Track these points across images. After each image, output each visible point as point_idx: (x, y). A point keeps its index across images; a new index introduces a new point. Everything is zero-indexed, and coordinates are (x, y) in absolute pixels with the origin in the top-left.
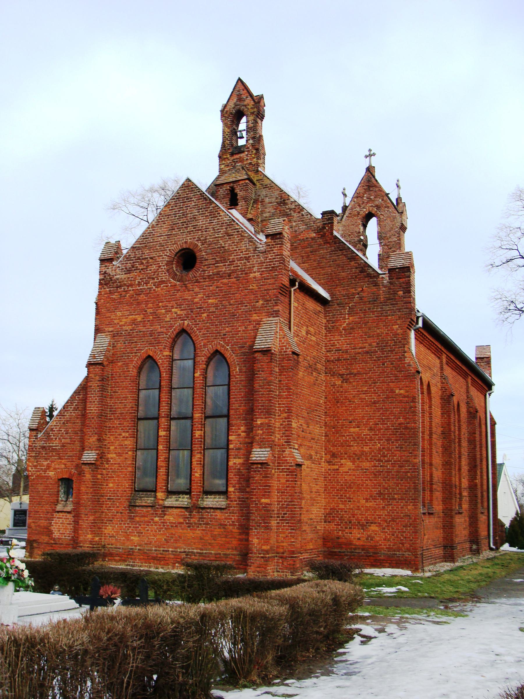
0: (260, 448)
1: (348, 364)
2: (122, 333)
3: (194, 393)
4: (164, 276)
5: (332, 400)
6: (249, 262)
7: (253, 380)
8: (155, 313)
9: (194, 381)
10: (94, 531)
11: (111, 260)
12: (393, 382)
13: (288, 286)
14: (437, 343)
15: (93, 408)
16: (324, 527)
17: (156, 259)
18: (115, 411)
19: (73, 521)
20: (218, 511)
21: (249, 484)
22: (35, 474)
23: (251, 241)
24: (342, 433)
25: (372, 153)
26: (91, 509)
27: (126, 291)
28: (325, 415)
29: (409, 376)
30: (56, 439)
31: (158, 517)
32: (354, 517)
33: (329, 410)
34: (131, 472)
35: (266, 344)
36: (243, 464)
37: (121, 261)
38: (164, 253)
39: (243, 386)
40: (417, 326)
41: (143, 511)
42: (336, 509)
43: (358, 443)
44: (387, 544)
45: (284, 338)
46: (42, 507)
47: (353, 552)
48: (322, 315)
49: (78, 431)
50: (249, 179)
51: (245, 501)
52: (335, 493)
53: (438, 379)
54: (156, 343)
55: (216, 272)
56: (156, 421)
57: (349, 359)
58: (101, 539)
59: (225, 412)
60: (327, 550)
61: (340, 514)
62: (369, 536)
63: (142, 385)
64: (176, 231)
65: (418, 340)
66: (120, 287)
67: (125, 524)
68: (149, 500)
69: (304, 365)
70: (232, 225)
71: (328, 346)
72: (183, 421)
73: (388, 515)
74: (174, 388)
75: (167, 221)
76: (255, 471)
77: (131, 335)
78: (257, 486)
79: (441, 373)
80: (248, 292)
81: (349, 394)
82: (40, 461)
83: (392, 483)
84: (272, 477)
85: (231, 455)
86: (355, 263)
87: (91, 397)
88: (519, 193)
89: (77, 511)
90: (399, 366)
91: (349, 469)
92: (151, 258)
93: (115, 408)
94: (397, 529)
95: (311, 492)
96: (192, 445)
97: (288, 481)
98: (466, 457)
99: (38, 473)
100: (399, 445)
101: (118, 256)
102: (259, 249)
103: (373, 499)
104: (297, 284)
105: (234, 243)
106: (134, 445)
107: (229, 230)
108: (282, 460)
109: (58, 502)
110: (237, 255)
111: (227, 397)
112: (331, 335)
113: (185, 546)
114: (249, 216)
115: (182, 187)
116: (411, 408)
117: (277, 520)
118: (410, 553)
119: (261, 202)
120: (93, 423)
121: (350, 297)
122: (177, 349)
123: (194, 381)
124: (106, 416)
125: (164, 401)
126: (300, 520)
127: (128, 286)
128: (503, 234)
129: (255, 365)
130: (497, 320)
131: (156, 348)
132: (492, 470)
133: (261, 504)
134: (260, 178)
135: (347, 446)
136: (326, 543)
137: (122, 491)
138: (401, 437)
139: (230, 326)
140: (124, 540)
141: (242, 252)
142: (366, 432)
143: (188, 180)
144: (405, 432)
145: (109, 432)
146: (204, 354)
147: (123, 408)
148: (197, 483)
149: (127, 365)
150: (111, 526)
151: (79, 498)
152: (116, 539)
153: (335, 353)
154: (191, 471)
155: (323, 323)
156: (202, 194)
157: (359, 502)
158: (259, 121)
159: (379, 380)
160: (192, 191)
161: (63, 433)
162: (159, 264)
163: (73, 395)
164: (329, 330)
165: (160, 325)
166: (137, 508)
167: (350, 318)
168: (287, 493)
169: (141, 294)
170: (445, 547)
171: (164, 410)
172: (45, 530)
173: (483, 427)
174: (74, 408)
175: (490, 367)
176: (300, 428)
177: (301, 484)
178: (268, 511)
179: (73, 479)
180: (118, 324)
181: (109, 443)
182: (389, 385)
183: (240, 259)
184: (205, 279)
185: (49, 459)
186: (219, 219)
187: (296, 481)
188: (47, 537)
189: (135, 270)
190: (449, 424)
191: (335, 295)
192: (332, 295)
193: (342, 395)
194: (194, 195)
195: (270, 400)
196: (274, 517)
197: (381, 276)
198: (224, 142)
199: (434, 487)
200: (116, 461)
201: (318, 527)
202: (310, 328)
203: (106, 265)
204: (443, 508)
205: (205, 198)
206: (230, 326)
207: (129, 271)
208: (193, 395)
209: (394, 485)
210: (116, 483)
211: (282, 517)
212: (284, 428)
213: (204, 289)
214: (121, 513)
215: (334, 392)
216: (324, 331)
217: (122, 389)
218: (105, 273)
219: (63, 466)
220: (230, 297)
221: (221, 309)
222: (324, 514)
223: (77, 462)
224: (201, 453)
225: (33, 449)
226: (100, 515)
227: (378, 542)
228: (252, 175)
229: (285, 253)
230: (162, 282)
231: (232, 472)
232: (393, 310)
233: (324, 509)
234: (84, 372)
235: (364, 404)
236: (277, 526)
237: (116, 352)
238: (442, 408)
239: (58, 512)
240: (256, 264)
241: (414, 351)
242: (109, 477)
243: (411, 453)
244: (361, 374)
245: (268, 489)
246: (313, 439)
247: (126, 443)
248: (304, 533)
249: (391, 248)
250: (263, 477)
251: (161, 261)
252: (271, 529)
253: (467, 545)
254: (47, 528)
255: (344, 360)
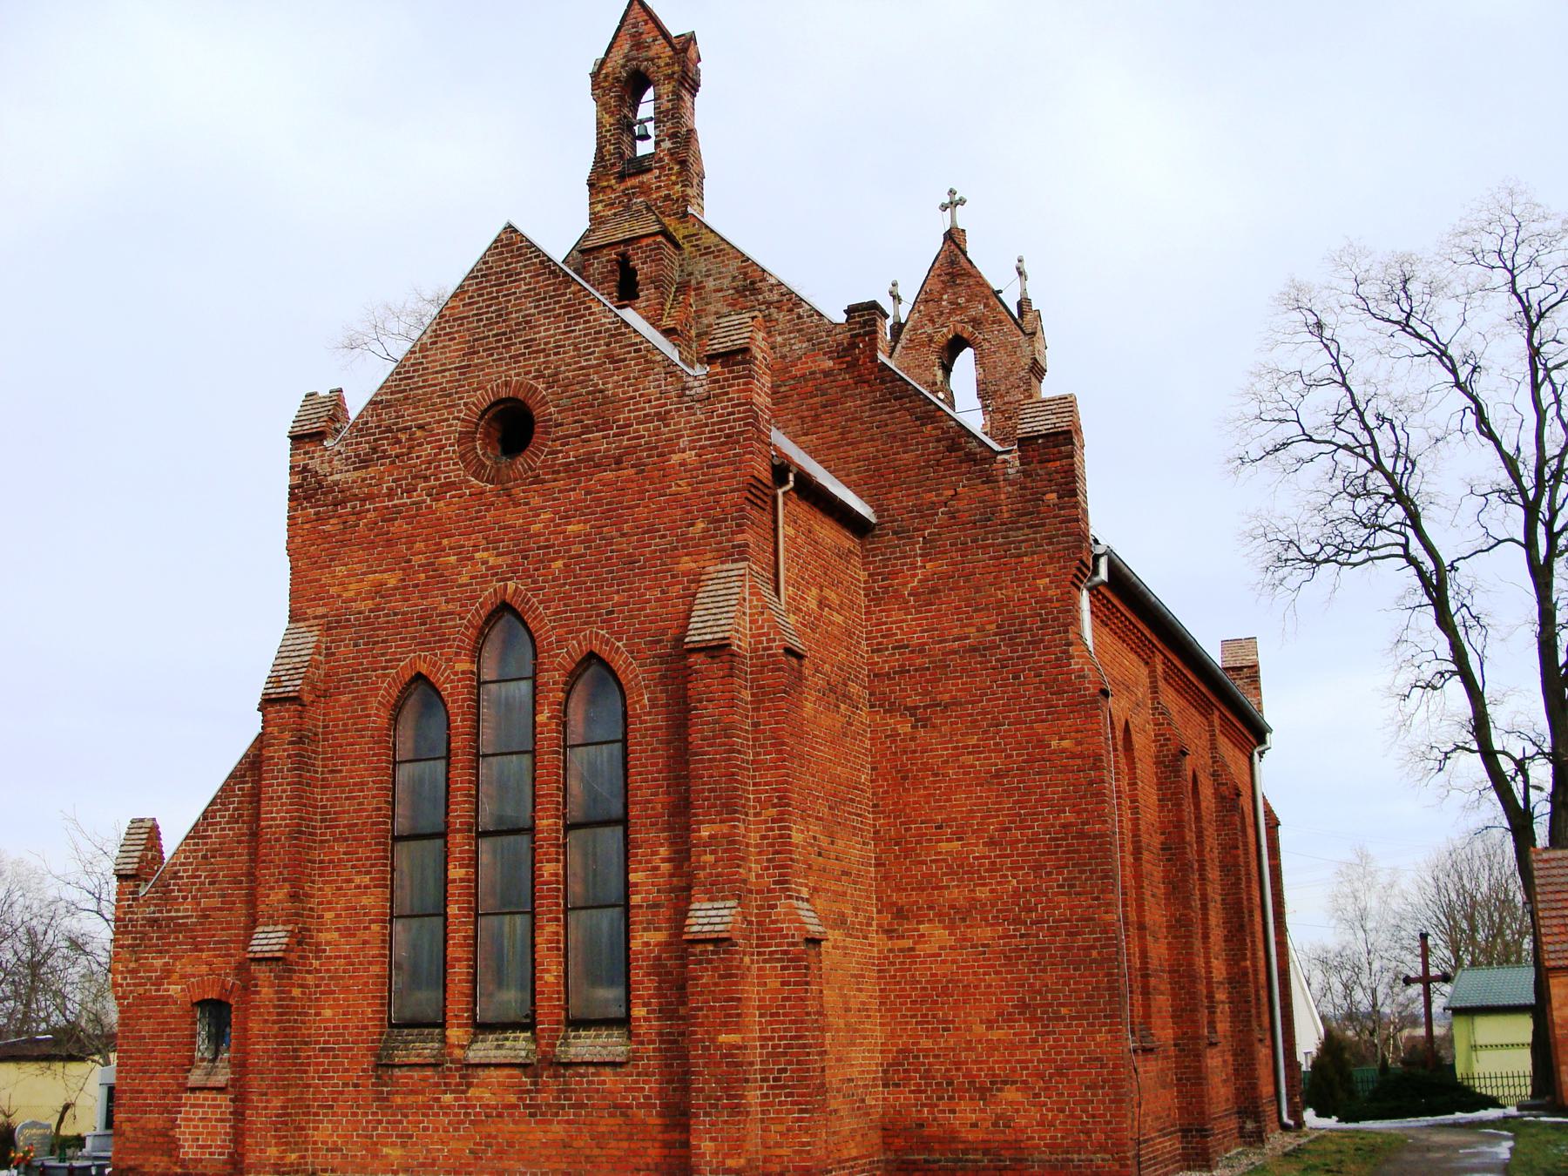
0: (711, 900)
1: (927, 681)
2: (349, 620)
3: (534, 764)
4: (454, 471)
5: (890, 773)
6: (667, 425)
7: (686, 726)
8: (432, 564)
9: (534, 735)
10: (286, 1137)
11: (318, 436)
12: (1042, 721)
13: (770, 484)
14: (1141, 626)
15: (277, 815)
16: (885, 1099)
17: (433, 430)
18: (335, 820)
19: (231, 1113)
20: (608, 1070)
21: (685, 995)
22: (131, 992)
23: (672, 374)
24: (919, 855)
25: (957, 197)
26: (275, 1079)
27: (359, 513)
28: (874, 812)
29: (1083, 703)
30: (185, 898)
31: (453, 1092)
32: (958, 1070)
33: (883, 799)
34: (378, 976)
35: (715, 629)
36: (668, 944)
37: (344, 439)
38: (452, 413)
39: (661, 742)
40: (1096, 579)
41: (411, 1077)
42: (911, 1051)
43: (961, 880)
44: (1048, 1136)
45: (763, 613)
46: (152, 1078)
47: (960, 1160)
48: (856, 561)
49: (242, 875)
50: (664, 233)
51: (676, 1042)
52: (907, 1010)
53: (1146, 714)
54: (435, 642)
55: (584, 454)
56: (440, 842)
57: (928, 669)
58: (303, 1157)
59: (616, 809)
60: (892, 1156)
61: (923, 1064)
62: (999, 1117)
63: (405, 748)
64: (482, 358)
65: (1097, 617)
66: (343, 503)
67: (366, 1114)
68: (428, 1049)
69: (816, 684)
70: (624, 334)
71: (876, 638)
72: (512, 838)
73: (1046, 1061)
74: (485, 756)
75: (457, 332)
76: (699, 962)
77: (373, 624)
78: (707, 1001)
79: (1153, 699)
80: (666, 502)
81: (933, 757)
82: (147, 958)
83: (1050, 977)
84: (743, 976)
85: (635, 923)
86: (935, 428)
87: (271, 785)
88: (1293, 293)
89: (241, 1086)
90: (1056, 680)
91: (941, 948)
92: (421, 427)
93: (335, 813)
94: (1069, 1095)
95: (848, 1010)
96: (533, 901)
97: (788, 983)
98: (1219, 906)
99: (141, 990)
100: (1064, 880)
101: (338, 426)
102: (693, 392)
103: (1004, 1021)
104: (791, 477)
105: (627, 379)
106: (384, 907)
107: (614, 349)
108: (768, 930)
109: (192, 1063)
110: (637, 410)
111: (621, 772)
112: (881, 611)
113: (524, 1166)
114: (668, 323)
115: (496, 248)
116: (1091, 783)
117: (761, 1088)
118: (1108, 1156)
119: (695, 290)
120: (279, 854)
121: (925, 512)
122: (490, 654)
123: (534, 735)
124: (311, 834)
125: (459, 789)
126: (823, 1084)
127: (363, 500)
128: (1263, 386)
129: (689, 686)
130: (1260, 586)
131: (436, 655)
132: (1276, 936)
133: (719, 1048)
134: (692, 230)
135: (933, 889)
136: (891, 1140)
137: (357, 1027)
138: (1068, 859)
139: (623, 591)
140: (363, 1157)
141: (650, 401)
142: (980, 850)
143: (510, 229)
144: (1079, 845)
145: (320, 875)
146: (560, 663)
147: (355, 811)
148: (550, 999)
149: (363, 700)
150: (330, 1121)
151: (245, 1052)
152: (345, 1156)
153: (894, 654)
154: (534, 967)
155: (859, 581)
156: (546, 262)
157: (969, 1029)
158: (687, 97)
159: (1009, 717)
160: (520, 255)
161: (202, 883)
162: (441, 440)
163: (226, 783)
164: (874, 598)
165: (445, 595)
166: (397, 1072)
167: (928, 565)
168: (785, 1015)
169: (396, 519)
170: (1185, 1132)
171: (460, 812)
172: (160, 1139)
173: (1250, 831)
174: (232, 816)
175: (1258, 688)
176: (811, 845)
177: (821, 991)
178: (737, 1064)
179: (232, 1001)
180: (339, 596)
181: (321, 903)
182: (1032, 728)
183: (646, 419)
184: (559, 472)
185: (168, 951)
186: (589, 321)
187: (807, 983)
188: (165, 1158)
189: (378, 458)
190: (1179, 825)
191: (888, 510)
192: (878, 510)
193: (916, 758)
194: (525, 266)
195: (733, 774)
196: (755, 1080)
197: (999, 457)
198: (600, 148)
199: (1153, 981)
200: (340, 950)
201: (869, 1101)
202: (827, 592)
203: (307, 448)
204: (1174, 1033)
205: (552, 272)
206: (623, 591)
207: (364, 462)
208: (534, 770)
209: (1057, 984)
210: (340, 1006)
211: (775, 1079)
212: (772, 845)
213: (554, 499)
214: (356, 1085)
215: (895, 753)
216: (863, 601)
217: (353, 764)
218: (305, 469)
219: (204, 969)
220: (621, 515)
221: (599, 546)
222: (882, 1065)
223: (238, 955)
224: (558, 920)
225: (126, 926)
226: (302, 1093)
227: (1022, 1131)
228: (672, 224)
229: (757, 399)
230: (450, 485)
231: (640, 967)
232: (1035, 539)
233: (882, 1052)
234: (251, 725)
235: (973, 779)
236: (762, 1104)
237: (334, 667)
238: (1160, 784)
239: (193, 1090)
240: (685, 429)
241: (1090, 643)
242: (322, 993)
243: (1097, 898)
244: (961, 704)
245: (737, 1008)
246: (845, 873)
247: (365, 901)
248: (834, 1116)
249: (1010, 418)
250: (721, 977)
251: (443, 434)
252: (748, 1113)
253: (1232, 1124)
254: (165, 1135)
255: (916, 670)
